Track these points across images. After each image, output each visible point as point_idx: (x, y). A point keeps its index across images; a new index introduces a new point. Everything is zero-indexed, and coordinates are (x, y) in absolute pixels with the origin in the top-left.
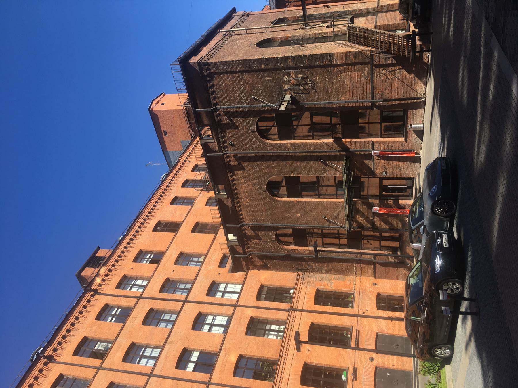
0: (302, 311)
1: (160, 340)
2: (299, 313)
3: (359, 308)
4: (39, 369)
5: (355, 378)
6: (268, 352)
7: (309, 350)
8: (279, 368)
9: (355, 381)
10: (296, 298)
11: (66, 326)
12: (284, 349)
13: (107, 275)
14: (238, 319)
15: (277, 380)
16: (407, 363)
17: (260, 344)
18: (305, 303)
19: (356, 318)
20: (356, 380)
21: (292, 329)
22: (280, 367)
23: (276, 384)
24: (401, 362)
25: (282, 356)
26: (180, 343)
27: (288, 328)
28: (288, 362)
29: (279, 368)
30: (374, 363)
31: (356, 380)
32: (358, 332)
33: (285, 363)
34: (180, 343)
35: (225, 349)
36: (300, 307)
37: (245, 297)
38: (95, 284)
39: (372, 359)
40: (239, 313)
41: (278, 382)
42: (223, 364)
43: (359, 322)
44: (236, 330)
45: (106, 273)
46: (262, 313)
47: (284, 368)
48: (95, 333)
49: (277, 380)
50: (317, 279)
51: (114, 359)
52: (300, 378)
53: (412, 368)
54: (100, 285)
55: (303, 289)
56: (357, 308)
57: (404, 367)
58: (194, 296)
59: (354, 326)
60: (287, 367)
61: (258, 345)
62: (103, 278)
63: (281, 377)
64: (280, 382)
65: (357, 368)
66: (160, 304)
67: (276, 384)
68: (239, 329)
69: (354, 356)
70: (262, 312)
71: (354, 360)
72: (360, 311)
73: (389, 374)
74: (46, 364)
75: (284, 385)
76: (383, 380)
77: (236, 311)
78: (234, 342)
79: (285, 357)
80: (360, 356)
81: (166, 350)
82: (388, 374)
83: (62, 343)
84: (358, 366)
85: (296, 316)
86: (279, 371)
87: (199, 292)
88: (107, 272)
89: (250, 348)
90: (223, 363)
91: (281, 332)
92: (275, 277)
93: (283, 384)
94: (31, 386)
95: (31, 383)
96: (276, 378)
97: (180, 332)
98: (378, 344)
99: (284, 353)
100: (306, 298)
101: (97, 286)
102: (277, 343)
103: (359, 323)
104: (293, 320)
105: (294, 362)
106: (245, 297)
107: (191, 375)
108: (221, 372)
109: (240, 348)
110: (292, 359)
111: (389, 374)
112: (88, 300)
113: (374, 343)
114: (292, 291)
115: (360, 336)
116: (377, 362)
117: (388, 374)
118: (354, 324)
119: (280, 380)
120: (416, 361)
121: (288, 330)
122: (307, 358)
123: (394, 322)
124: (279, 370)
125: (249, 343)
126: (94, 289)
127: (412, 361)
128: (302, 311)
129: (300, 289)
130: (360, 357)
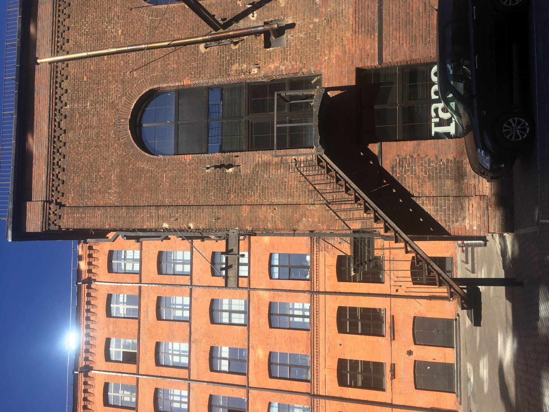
0: (325, 293)
1: (184, 339)
2: (322, 296)
3: (391, 283)
4: (82, 382)
5: (393, 376)
6: (298, 348)
7: (341, 345)
8: (314, 369)
9: (393, 342)
10: (315, 274)
11: (83, 308)
12: (314, 345)
13: (90, 256)
14: (256, 307)
15: (314, 383)
16: (448, 355)
17: (287, 339)
18: (327, 281)
19: (388, 299)
20: (394, 378)
21: (318, 319)
22: (314, 367)
23: (314, 387)
24: (443, 355)
25: (314, 354)
26: (204, 341)
27: (313, 312)
28: (322, 360)
29: (314, 369)
30: (413, 358)
31: (394, 378)
32: (393, 318)
33: (318, 342)
34: (204, 341)
35: (253, 347)
36: (322, 289)
37: (256, 276)
38: (84, 271)
39: (410, 353)
40: (256, 299)
41: (315, 385)
42: (255, 365)
43: (392, 304)
44: (257, 323)
45: (87, 253)
46: (281, 298)
47: (318, 367)
48: (114, 333)
49: (314, 383)
50: (336, 241)
51: (146, 363)
52: (336, 378)
53: (455, 362)
54: (90, 271)
55: (322, 259)
56: (389, 283)
57: (445, 360)
58: (198, 278)
59: (387, 309)
60: (322, 367)
61: (286, 340)
62: (88, 261)
63: (317, 378)
64: (317, 384)
65: (394, 364)
66: (165, 290)
67: (314, 387)
68: (260, 321)
69: (390, 349)
70: (281, 296)
71: (390, 354)
72: (392, 287)
73: (429, 367)
74: (89, 287)
75: (322, 388)
76: (423, 375)
77: (251, 297)
78: (259, 337)
79: (317, 355)
80: (397, 349)
81: (193, 351)
82: (429, 368)
83: (88, 389)
84: (395, 361)
85: (320, 301)
86: (314, 372)
87: (201, 270)
88: (88, 251)
89: (278, 344)
90: (255, 364)
91: (307, 317)
92: (284, 241)
93: (321, 388)
94: (85, 407)
95: (87, 292)
96: (313, 381)
97: (200, 328)
98: (415, 330)
99: (315, 351)
100: (326, 272)
101: (87, 274)
102: (305, 336)
103: (392, 306)
104: (317, 305)
105: (327, 360)
106: (256, 276)
107: (228, 378)
108: (256, 373)
109: (268, 344)
110: (324, 357)
111: (429, 367)
112: (84, 382)
113: (412, 332)
114: (308, 258)
115: (395, 323)
116: (416, 356)
117: (429, 368)
118: (386, 306)
119: (317, 381)
120: (459, 377)
121: (314, 321)
122: (341, 355)
123: (433, 302)
124: (314, 370)
125: (275, 338)
126: (86, 278)
127: (454, 353)
128: (325, 293)
129: (317, 259)
130: (397, 351)
